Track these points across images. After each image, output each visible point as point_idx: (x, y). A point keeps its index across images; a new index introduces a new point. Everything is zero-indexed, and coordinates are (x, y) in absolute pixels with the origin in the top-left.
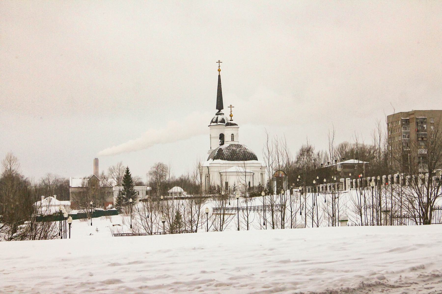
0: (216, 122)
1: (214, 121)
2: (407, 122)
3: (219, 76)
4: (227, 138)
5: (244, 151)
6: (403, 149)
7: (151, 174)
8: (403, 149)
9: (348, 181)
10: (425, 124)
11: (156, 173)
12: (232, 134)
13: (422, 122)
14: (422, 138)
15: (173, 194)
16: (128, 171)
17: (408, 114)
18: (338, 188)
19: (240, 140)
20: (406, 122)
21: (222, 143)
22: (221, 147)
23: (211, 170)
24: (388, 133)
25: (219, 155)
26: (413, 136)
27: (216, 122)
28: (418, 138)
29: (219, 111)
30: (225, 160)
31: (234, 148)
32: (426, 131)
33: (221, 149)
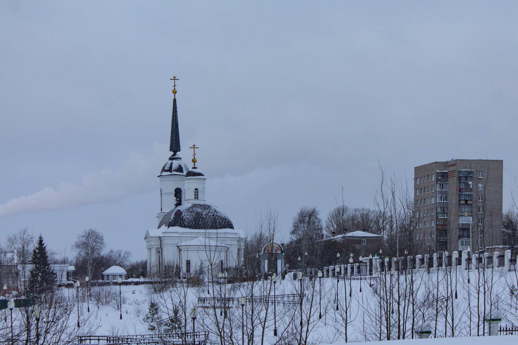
0: (170, 170)
1: (166, 169)
2: (444, 176)
3: (175, 100)
4: (188, 196)
5: (214, 215)
6: (437, 217)
7: (78, 246)
8: (437, 217)
9: (376, 260)
10: (472, 180)
11: (85, 245)
12: (196, 189)
13: (466, 177)
14: (466, 201)
15: (110, 277)
16: (41, 242)
17: (446, 164)
18: (359, 272)
19: (206, 199)
20: (443, 176)
21: (179, 203)
22: (179, 208)
23: (165, 242)
24: (415, 193)
25: (177, 220)
26: (453, 199)
27: (170, 170)
28: (460, 201)
29: (174, 155)
30: (185, 227)
31: (199, 210)
32: (471, 190)
33: (179, 210)
